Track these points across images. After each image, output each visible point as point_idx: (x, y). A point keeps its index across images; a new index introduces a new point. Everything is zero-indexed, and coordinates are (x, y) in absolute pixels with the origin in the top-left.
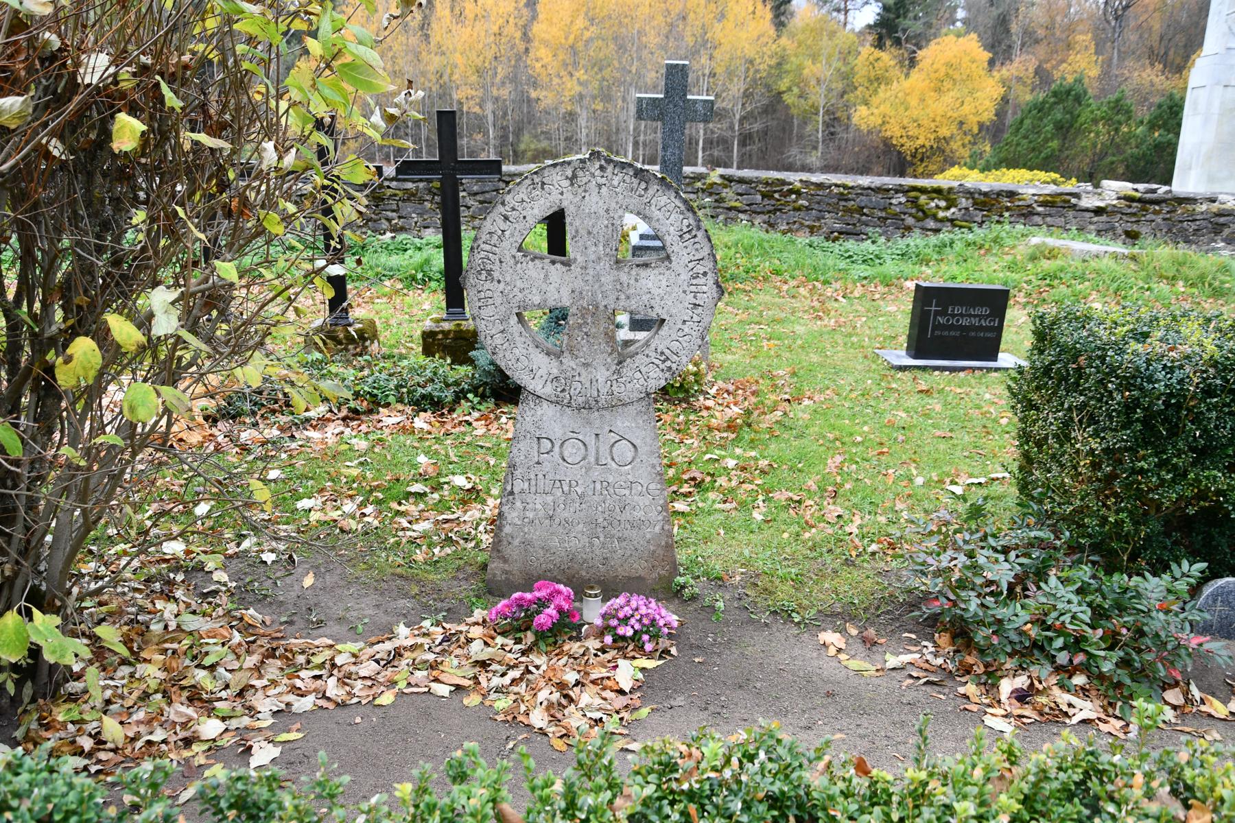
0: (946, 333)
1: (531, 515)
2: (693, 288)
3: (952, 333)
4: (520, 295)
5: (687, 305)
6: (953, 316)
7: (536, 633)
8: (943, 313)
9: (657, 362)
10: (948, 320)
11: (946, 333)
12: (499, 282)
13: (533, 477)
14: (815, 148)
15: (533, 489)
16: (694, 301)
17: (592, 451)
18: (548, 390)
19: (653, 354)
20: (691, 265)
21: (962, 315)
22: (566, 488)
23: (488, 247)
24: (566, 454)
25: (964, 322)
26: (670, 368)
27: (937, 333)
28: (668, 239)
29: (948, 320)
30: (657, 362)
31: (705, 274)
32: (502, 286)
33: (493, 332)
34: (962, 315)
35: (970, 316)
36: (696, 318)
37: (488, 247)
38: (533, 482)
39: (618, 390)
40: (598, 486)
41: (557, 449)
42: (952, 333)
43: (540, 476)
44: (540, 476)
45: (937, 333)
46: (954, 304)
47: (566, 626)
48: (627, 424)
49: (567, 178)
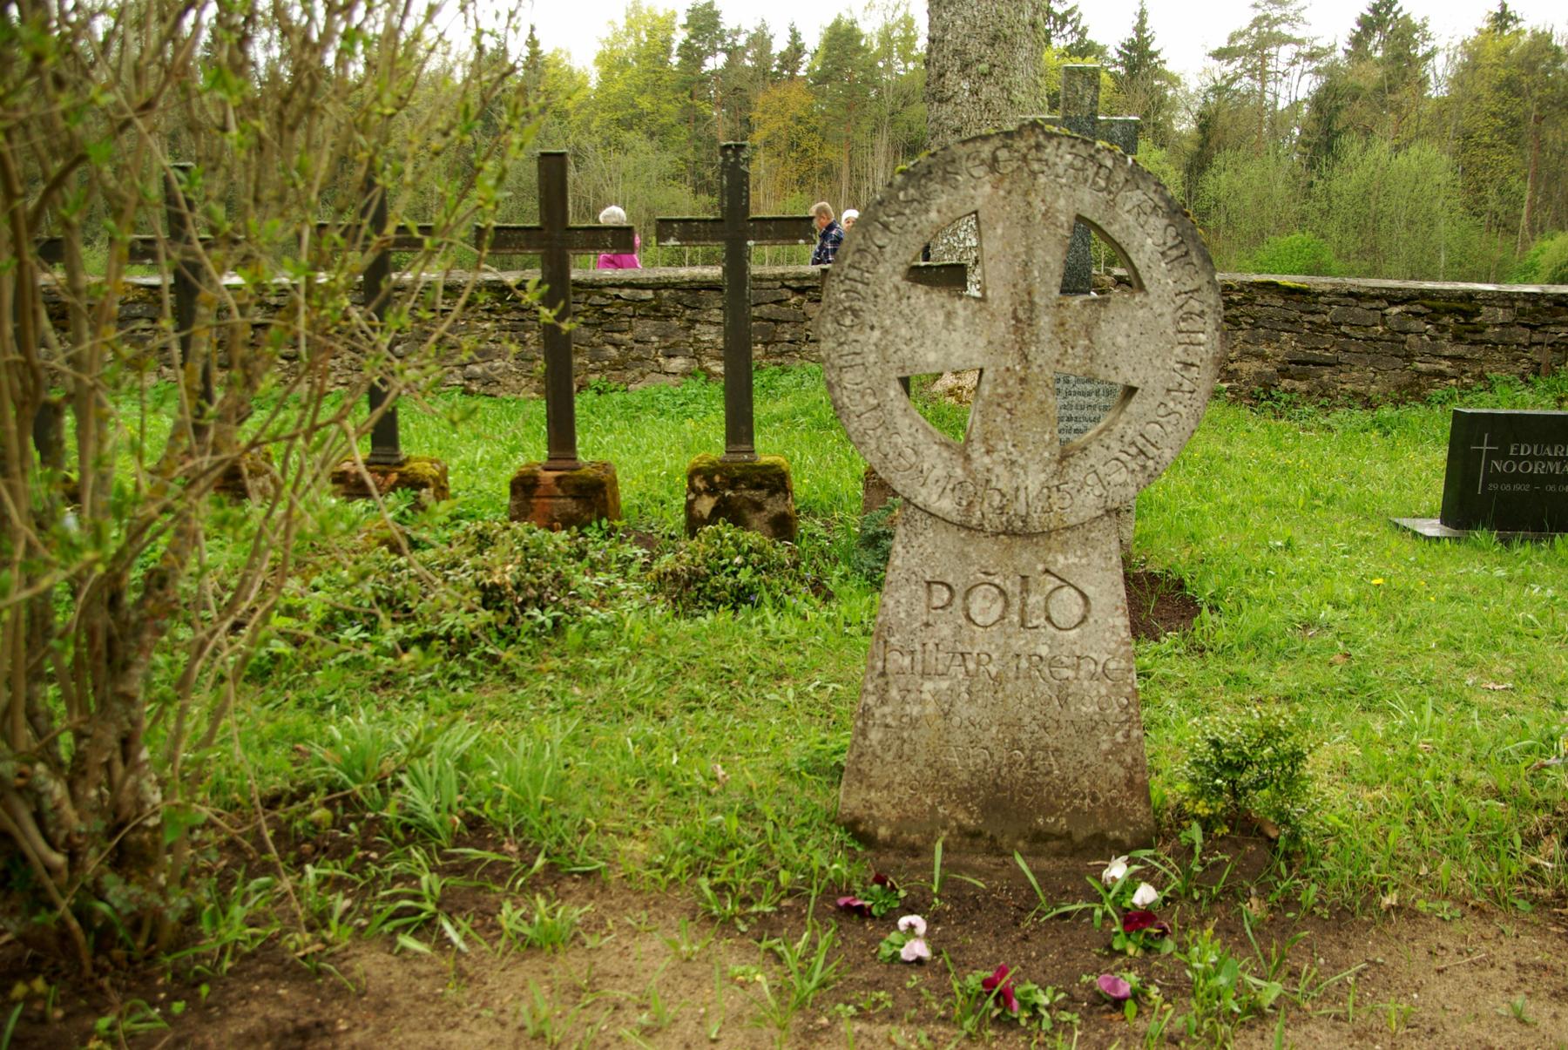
0: (1507, 487)
1: (915, 710)
2: (1182, 337)
3: (1518, 487)
4: (906, 350)
5: (1172, 364)
6: (1518, 459)
7: (401, 475)
8: (1503, 455)
9: (1124, 457)
10: (1509, 467)
11: (1507, 487)
12: (872, 328)
13: (918, 647)
14: (947, 971)
15: (919, 668)
16: (1184, 358)
17: (1016, 602)
18: (946, 505)
19: (1116, 446)
20: (1179, 301)
21: (1532, 458)
22: (971, 666)
23: (855, 274)
24: (975, 611)
25: (1536, 469)
26: (1144, 467)
27: (1492, 487)
28: (1140, 260)
29: (1509, 467)
30: (1124, 457)
31: (1202, 314)
32: (877, 333)
33: (862, 408)
34: (1532, 458)
35: (1546, 459)
36: (1187, 386)
37: (855, 274)
38: (918, 656)
39: (1059, 504)
40: (1024, 664)
41: (958, 601)
42: (1518, 487)
43: (931, 646)
44: (931, 646)
45: (1492, 487)
46: (1518, 440)
47: (1252, 53)
48: (1072, 560)
49: (983, 162)
